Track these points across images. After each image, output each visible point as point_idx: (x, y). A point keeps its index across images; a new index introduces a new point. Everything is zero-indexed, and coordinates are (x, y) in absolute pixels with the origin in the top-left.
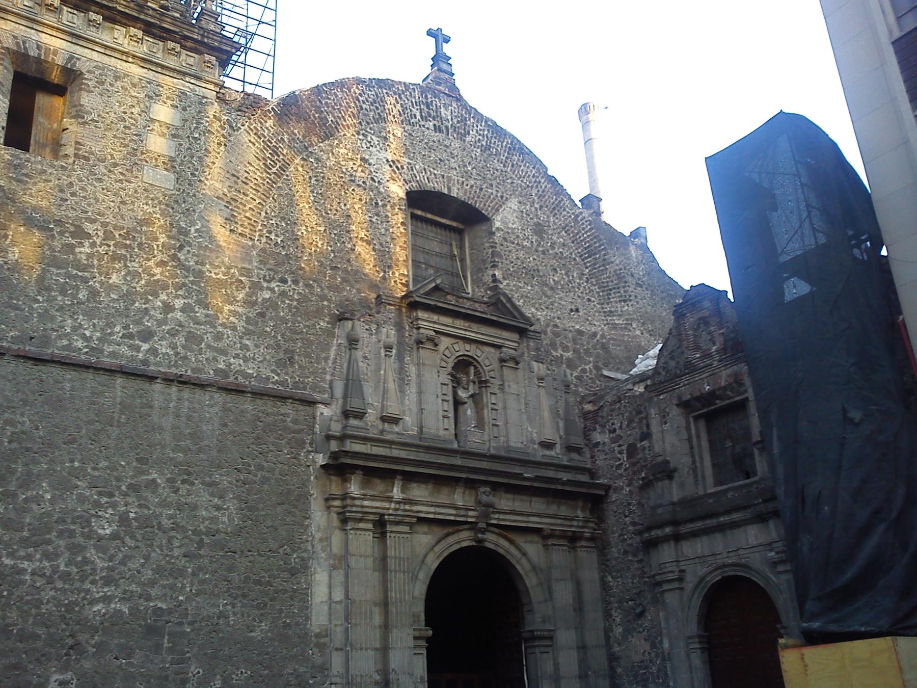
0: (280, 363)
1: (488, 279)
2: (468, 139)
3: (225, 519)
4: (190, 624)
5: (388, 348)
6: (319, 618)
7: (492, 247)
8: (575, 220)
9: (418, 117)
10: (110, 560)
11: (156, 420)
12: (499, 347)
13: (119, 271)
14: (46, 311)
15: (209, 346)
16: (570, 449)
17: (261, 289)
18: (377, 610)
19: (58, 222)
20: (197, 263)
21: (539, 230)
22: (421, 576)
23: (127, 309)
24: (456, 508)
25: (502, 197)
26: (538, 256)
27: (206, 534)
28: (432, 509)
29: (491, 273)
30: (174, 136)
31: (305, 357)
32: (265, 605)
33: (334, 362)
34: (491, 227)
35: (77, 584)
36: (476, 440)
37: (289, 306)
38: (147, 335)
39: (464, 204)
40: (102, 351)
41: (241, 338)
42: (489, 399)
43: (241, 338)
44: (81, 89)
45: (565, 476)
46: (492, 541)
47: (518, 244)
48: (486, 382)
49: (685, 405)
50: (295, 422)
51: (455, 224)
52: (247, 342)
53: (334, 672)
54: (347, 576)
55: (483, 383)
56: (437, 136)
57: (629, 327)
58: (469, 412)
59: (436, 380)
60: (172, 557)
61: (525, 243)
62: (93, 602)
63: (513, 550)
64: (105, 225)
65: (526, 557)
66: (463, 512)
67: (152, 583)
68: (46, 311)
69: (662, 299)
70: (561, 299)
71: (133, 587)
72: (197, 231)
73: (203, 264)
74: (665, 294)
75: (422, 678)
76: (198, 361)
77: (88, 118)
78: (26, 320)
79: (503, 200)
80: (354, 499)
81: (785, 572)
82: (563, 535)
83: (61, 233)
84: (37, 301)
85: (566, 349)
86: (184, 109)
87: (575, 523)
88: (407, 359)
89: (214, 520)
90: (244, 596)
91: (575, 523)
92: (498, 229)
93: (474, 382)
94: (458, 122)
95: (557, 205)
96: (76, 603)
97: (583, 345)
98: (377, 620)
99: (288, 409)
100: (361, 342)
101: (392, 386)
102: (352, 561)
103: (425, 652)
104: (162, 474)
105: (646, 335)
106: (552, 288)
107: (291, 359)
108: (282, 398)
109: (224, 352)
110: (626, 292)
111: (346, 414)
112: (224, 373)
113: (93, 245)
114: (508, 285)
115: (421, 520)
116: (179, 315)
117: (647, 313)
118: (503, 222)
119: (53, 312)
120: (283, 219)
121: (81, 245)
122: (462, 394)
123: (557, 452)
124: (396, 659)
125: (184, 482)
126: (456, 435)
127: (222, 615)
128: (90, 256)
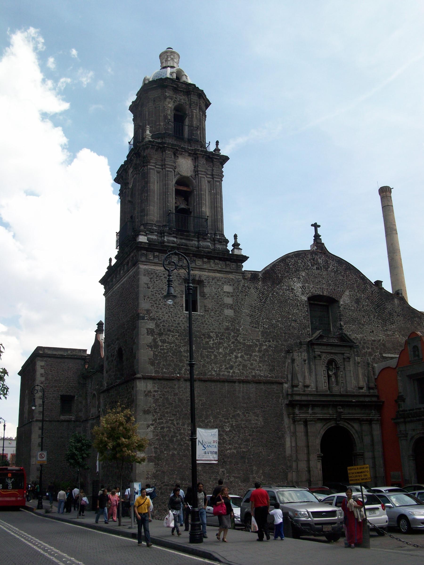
0: (271, 370)
1: (338, 325)
2: (329, 269)
3: (259, 423)
4: (252, 455)
5: (305, 361)
6: (288, 452)
7: (339, 312)
8: (372, 294)
9: (310, 265)
10: (230, 438)
11: (237, 394)
12: (343, 354)
13: (221, 347)
14: (204, 364)
15: (249, 368)
16: (369, 388)
17: (263, 346)
18: (305, 448)
19: (204, 335)
20: (243, 340)
21: (358, 301)
22: (319, 437)
23: (225, 360)
24: (330, 414)
25: (343, 291)
26: (357, 312)
27: (254, 428)
28: (322, 415)
29: (339, 323)
30: (232, 296)
31: (278, 367)
32: (272, 448)
33: (288, 367)
34: (339, 304)
35: (222, 445)
36: (336, 389)
37: (272, 350)
38: (232, 367)
39: (329, 297)
40: (220, 375)
41: (258, 364)
42: (341, 374)
43: (258, 364)
44: (203, 287)
45: (367, 399)
46: (342, 424)
47: (349, 309)
48: (339, 367)
49: (410, 377)
50: (277, 390)
51: (325, 304)
52: (260, 365)
53: (294, 468)
54: (296, 439)
55: (337, 368)
56: (317, 272)
57: (394, 334)
58: (333, 380)
59: (321, 369)
60: (246, 436)
61: (352, 308)
62: (227, 450)
63: (349, 426)
64: (216, 333)
65: (354, 428)
66: (332, 415)
67: (241, 444)
68: (204, 364)
69: (408, 319)
70: (366, 328)
71: (236, 445)
72: (242, 329)
73: (245, 340)
74: (409, 317)
75: (320, 469)
76: (247, 373)
77: (207, 296)
78: (199, 368)
79: (343, 292)
80: (297, 414)
81: (352, 480)
82: (367, 420)
83: (205, 338)
84: (201, 362)
85: (368, 348)
86: (233, 285)
87: (371, 415)
88: (311, 363)
89: (256, 424)
90: (266, 446)
91: (371, 415)
92: (342, 305)
93: (334, 368)
94: (325, 263)
95: (364, 289)
96: (223, 450)
97: (375, 345)
98: (306, 452)
99: (274, 386)
100: (296, 361)
101: (307, 374)
102: (298, 434)
103: (321, 461)
104: (240, 411)
105: (401, 336)
106: (363, 325)
107: (274, 369)
108: (272, 383)
109: (254, 369)
110: (393, 320)
111: (293, 386)
112: (254, 376)
113: (213, 340)
114: (346, 327)
115: (319, 419)
116: (240, 359)
117: (401, 327)
118: (343, 301)
119: (206, 364)
120: (268, 318)
121: (210, 341)
122: (330, 373)
123: (364, 391)
124: (312, 463)
125: (247, 413)
126: (329, 388)
127: (261, 452)
128: (213, 344)
